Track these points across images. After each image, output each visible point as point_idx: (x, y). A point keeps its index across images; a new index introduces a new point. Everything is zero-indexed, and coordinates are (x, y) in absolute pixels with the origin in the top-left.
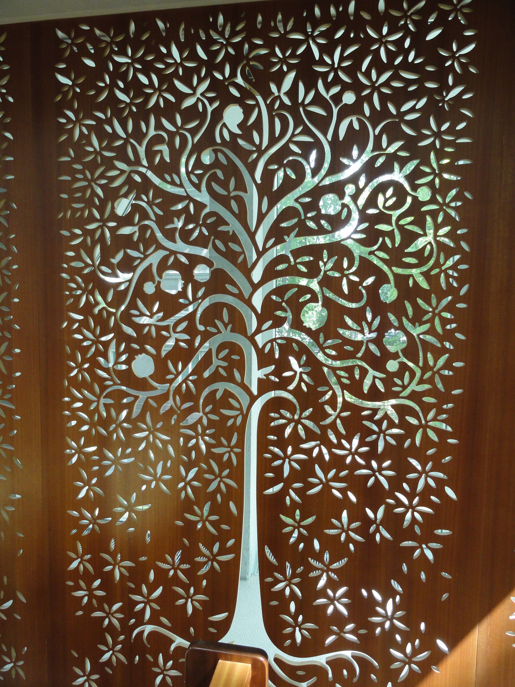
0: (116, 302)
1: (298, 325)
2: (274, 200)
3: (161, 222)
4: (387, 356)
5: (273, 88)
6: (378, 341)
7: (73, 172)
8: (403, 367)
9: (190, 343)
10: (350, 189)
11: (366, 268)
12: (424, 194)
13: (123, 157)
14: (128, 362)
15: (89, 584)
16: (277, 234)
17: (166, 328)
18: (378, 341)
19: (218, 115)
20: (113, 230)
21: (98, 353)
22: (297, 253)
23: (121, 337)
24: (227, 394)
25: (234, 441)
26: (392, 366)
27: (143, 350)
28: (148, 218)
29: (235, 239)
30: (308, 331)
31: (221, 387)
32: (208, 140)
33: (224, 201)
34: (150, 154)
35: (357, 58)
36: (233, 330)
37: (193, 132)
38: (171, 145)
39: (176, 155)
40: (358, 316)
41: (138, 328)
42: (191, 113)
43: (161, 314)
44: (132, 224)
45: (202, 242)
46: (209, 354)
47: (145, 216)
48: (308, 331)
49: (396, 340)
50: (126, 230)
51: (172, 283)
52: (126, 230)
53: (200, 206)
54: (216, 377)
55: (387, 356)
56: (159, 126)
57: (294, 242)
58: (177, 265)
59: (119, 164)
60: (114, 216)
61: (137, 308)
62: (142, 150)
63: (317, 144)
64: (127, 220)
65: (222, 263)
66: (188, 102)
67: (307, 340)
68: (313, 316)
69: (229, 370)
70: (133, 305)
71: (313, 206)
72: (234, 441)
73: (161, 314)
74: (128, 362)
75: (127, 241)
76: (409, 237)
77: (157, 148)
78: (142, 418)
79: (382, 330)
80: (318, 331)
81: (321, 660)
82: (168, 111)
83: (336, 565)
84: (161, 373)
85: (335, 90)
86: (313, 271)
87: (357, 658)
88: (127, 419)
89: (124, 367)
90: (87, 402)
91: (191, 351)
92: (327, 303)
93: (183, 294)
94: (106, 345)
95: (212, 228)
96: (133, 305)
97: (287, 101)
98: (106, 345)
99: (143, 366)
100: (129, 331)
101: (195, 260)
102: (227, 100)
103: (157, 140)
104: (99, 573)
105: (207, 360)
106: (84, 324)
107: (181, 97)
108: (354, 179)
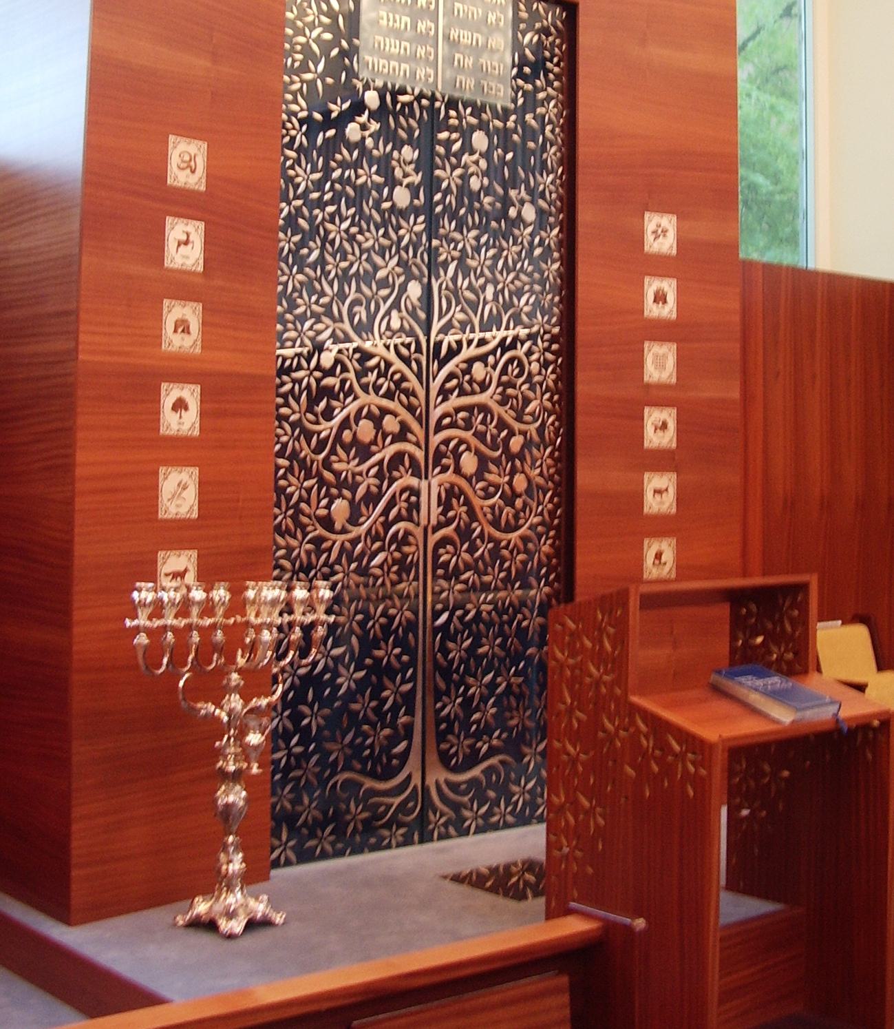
1: (458, 471)
40: (497, 462)
45: (389, 395)
51: (365, 430)
57: (455, 401)
64: (330, 372)
65: (405, 415)
68: (469, 463)
82: (368, 278)
86: (468, 426)
91: (380, 496)
101: (384, 411)
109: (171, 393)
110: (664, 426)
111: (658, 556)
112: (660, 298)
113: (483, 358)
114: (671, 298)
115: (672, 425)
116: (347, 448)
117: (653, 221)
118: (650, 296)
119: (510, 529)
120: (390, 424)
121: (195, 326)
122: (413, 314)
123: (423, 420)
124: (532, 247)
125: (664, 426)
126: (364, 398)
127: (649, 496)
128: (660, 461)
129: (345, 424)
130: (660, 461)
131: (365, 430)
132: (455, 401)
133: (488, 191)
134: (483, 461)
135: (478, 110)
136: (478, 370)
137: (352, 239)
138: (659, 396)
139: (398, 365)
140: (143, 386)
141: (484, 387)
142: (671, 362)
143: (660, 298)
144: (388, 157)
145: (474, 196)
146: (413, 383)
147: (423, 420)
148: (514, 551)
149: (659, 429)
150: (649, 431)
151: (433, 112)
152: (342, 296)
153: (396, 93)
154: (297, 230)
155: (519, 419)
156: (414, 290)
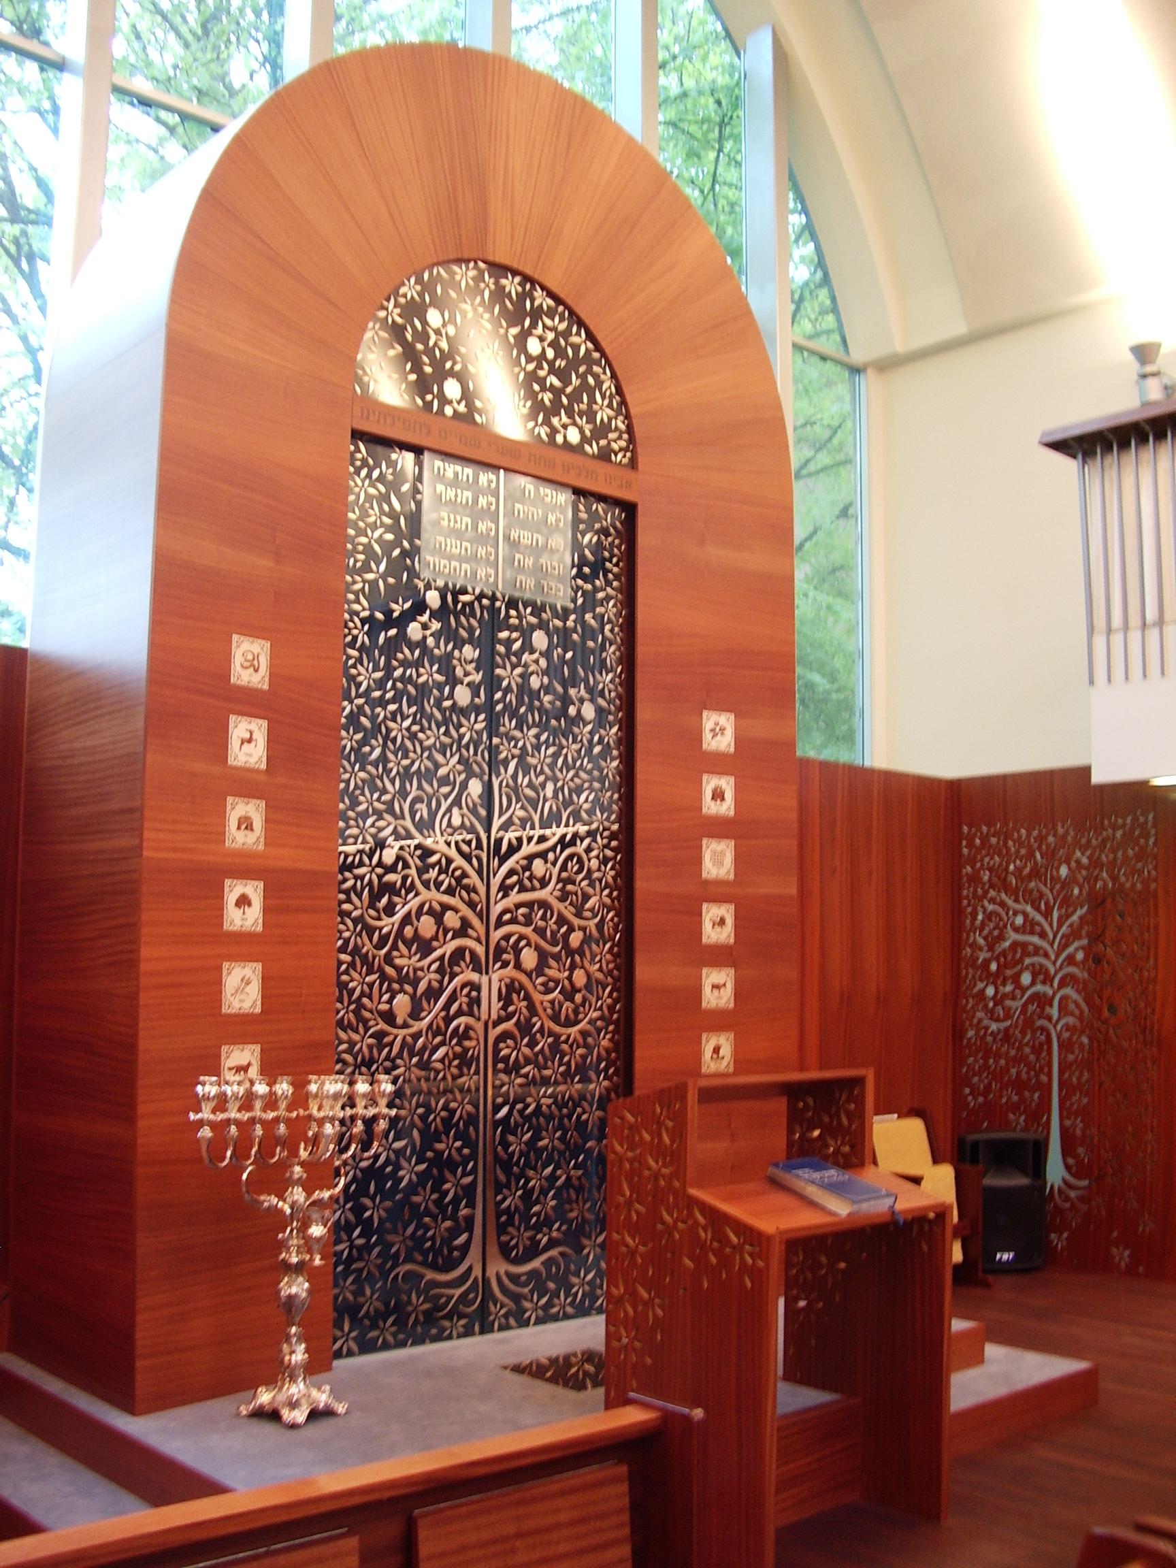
0: (380, 946)
1: (518, 966)
2: (502, 861)
3: (420, 872)
4: (575, 990)
5: (502, 770)
6: (570, 978)
7: (346, 820)
8: (585, 999)
9: (441, 982)
10: (551, 856)
11: (562, 920)
12: (594, 863)
13: (390, 810)
14: (390, 1001)
15: (350, 1235)
16: (505, 889)
17: (422, 969)
18: (570, 978)
19: (464, 785)
20: (380, 877)
21: (363, 994)
22: (518, 906)
23: (384, 977)
24: (468, 1028)
25: (472, 1071)
26: (578, 998)
27: (402, 990)
28: (409, 867)
29: (475, 890)
30: (525, 972)
31: (462, 1020)
32: (457, 802)
33: (467, 857)
34: (413, 813)
35: (555, 756)
36: (473, 970)
37: (446, 797)
38: (429, 805)
39: (432, 815)
40: (557, 957)
41: (399, 969)
42: (444, 781)
43: (418, 956)
44: (395, 871)
45: (450, 891)
46: (455, 991)
47: (406, 866)
48: (525, 972)
49: (579, 978)
50: (391, 877)
51: (427, 926)
52: (391, 877)
53: (449, 861)
54: (460, 1013)
55: (575, 990)
56: (420, 787)
57: (515, 897)
58: (431, 912)
59: (386, 816)
60: (380, 864)
61: (398, 950)
62: (406, 807)
63: (531, 819)
64: (392, 869)
65: (466, 911)
66: (442, 772)
67: (524, 979)
68: (529, 958)
69: (470, 1005)
70: (395, 947)
71: (528, 868)
72: (472, 1071)
73: (418, 956)
74: (390, 1001)
75: (390, 888)
76: (586, 897)
77: (418, 806)
78: (400, 1055)
79: (572, 968)
80: (531, 972)
81: (536, 1263)
82: (429, 775)
83: (346, 1328)
84: (415, 1014)
85: (542, 778)
86: (528, 921)
87: (562, 1254)
88: (387, 1058)
89: (386, 1007)
90: (352, 1044)
91: (441, 991)
92: (537, 948)
93: (435, 938)
94: (371, 986)
95: (458, 880)
96: (395, 947)
97: (511, 782)
98: (371, 986)
99: (402, 1003)
100: (390, 971)
101: (446, 907)
102: (471, 774)
103: (417, 800)
104: (360, 1221)
105: (453, 998)
106: (352, 965)
107: (437, 766)
108: (553, 849)
109: (234, 890)
110: (722, 922)
111: (716, 1050)
112: (718, 795)
113: (543, 855)
114: (729, 795)
115: (730, 921)
116: (408, 944)
117: (711, 720)
118: (708, 794)
119: (569, 1023)
120: (451, 920)
121: (258, 823)
122: (474, 811)
123: (484, 916)
124: (591, 745)
125: (722, 922)
126: (425, 894)
127: (707, 991)
128: (718, 956)
129: (407, 920)
130: (718, 956)
131: (427, 926)
132: (515, 897)
133: (548, 689)
134: (543, 956)
135: (538, 610)
136: (538, 867)
137: (413, 737)
138: (717, 892)
139: (459, 861)
140: (206, 882)
141: (544, 883)
142: (729, 859)
143: (718, 795)
144: (449, 656)
145: (534, 695)
146: (474, 879)
147: (484, 916)
148: (574, 1045)
149: (717, 925)
150: (707, 926)
151: (494, 611)
152: (403, 793)
153: (457, 593)
154: (359, 728)
155: (578, 915)
156: (475, 787)
